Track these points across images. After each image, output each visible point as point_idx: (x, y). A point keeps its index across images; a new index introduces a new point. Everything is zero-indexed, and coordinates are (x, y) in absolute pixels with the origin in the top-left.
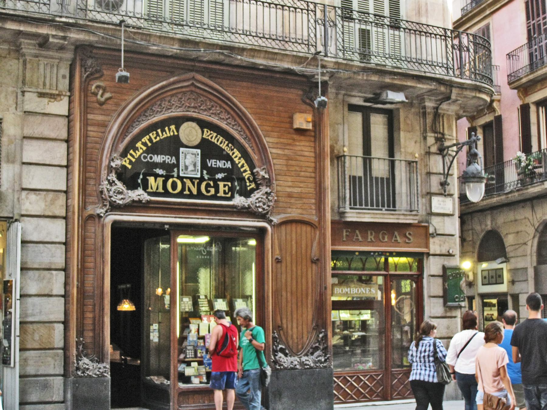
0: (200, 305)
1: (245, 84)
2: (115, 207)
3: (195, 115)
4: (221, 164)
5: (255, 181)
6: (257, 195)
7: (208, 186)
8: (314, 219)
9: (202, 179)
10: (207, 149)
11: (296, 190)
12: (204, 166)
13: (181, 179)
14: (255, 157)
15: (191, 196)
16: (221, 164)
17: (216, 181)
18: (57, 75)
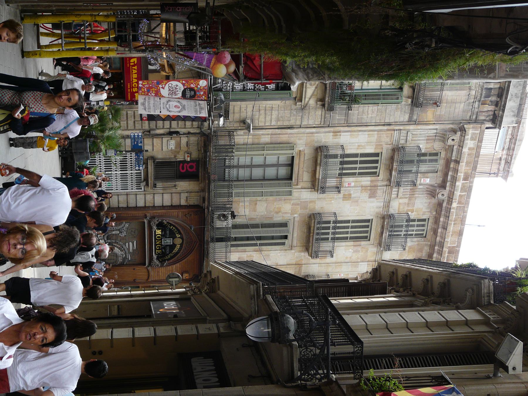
0: (194, 374)
1: (205, 264)
2: (149, 222)
3: (184, 242)
4: (168, 250)
5: (162, 261)
6: (157, 262)
7: (160, 247)
8: (150, 280)
9: (162, 245)
10: (173, 246)
11: (161, 274)
12: (167, 245)
13: (161, 239)
14: (171, 261)
15: (155, 242)
16: (168, 250)
17: (161, 249)
18: (194, 200)
